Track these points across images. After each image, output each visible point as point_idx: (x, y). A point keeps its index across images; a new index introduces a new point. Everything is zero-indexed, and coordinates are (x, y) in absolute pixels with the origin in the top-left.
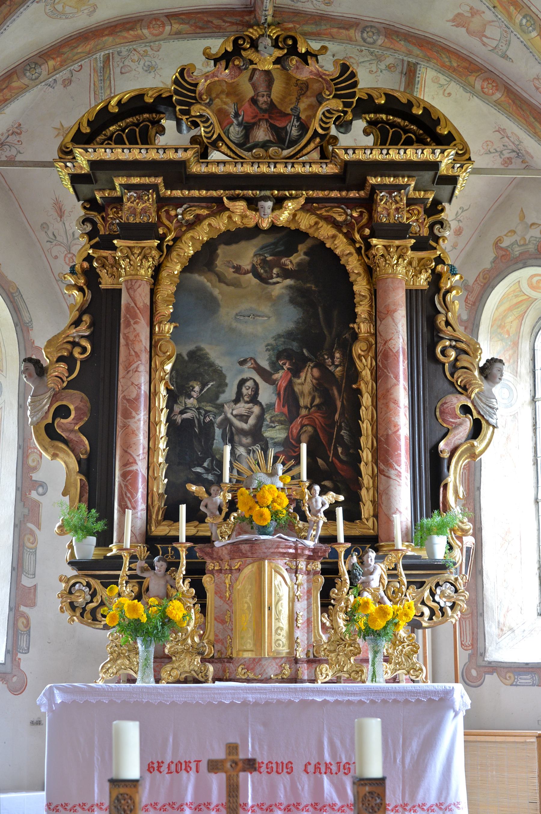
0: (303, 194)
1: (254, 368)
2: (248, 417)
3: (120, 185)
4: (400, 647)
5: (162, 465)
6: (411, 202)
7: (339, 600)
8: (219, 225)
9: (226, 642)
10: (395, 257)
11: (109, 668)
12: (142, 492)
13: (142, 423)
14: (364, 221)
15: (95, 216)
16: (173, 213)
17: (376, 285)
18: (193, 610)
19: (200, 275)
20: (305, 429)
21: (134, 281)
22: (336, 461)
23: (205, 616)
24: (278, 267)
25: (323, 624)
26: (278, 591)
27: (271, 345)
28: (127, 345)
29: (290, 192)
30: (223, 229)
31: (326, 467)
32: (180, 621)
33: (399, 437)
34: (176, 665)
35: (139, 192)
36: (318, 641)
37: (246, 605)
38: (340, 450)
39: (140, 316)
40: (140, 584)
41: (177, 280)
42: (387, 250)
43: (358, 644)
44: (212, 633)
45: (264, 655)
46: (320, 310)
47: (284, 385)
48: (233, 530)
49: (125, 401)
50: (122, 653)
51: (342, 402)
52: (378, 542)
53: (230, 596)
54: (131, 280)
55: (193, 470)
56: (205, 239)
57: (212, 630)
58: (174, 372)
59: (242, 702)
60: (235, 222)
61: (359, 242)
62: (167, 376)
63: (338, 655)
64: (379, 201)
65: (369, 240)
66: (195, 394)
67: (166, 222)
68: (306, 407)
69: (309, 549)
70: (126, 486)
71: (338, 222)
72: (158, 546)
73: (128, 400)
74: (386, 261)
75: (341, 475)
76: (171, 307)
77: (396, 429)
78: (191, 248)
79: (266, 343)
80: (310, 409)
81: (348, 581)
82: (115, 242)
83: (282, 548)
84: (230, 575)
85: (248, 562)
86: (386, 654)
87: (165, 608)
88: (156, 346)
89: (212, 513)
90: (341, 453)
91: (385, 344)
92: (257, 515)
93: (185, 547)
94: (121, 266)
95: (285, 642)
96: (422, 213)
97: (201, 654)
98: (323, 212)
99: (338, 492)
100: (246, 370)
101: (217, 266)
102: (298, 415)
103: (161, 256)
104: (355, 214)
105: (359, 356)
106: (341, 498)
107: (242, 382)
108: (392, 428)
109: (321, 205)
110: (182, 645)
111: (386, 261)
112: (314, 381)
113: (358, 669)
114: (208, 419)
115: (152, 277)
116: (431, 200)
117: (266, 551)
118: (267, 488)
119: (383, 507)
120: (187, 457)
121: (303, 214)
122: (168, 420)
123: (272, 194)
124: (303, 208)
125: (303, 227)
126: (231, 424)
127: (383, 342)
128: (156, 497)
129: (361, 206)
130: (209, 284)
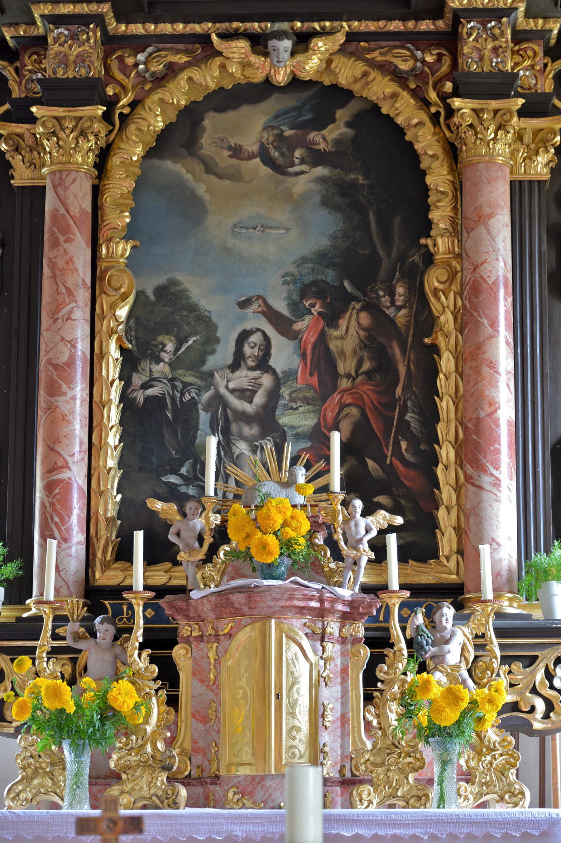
0: (342, 27)
1: (263, 313)
2: (254, 392)
3: (41, 16)
4: (489, 758)
5: (112, 472)
6: (523, 36)
7: (390, 683)
8: (205, 80)
9: (210, 751)
10: (492, 128)
11: (20, 792)
12: (79, 515)
13: (78, 402)
14: (445, 68)
15: (4, 68)
16: (130, 61)
17: (462, 174)
18: (154, 700)
19: (175, 162)
20: (346, 411)
21: (65, 173)
22: (397, 463)
23: (176, 711)
24: (302, 147)
25: (368, 724)
26: (292, 668)
27: (292, 274)
28: (54, 276)
29: (322, 23)
30: (213, 86)
31: (381, 473)
32: (131, 715)
33: (497, 422)
34: (128, 787)
35: (73, 27)
36: (360, 751)
37: (241, 692)
38: (404, 445)
39: (74, 228)
40: (74, 661)
41: (138, 171)
42: (478, 117)
43: (421, 753)
44: (188, 738)
45: (270, 771)
46: (372, 216)
47: (313, 340)
48: (223, 573)
49: (51, 368)
50: (41, 768)
51: (408, 366)
52: (463, 594)
53: (215, 677)
54: (60, 171)
55: (164, 479)
56: (183, 103)
57: (189, 733)
58: (132, 321)
59: (225, 838)
60: (232, 75)
61: (437, 105)
62: (121, 327)
63: (389, 770)
64: (465, 36)
65: (448, 101)
66: (166, 357)
67: (119, 76)
68: (348, 376)
69: (344, 602)
70: (52, 504)
71: (401, 71)
72: (107, 603)
73: (56, 367)
74: (476, 135)
75: (405, 486)
76: (127, 214)
77: (493, 409)
78: (159, 119)
79: (283, 272)
80: (354, 379)
81: (405, 652)
82: (34, 109)
83: (298, 599)
84: (215, 644)
85: (243, 623)
86: (465, 768)
87: (107, 692)
88: (102, 279)
89: (187, 545)
90: (406, 450)
91: (475, 270)
92: (257, 546)
93: (142, 598)
94: (45, 148)
95: (303, 751)
96: (541, 54)
97: (167, 768)
98: (376, 55)
99: (393, 511)
100: (251, 315)
101: (202, 147)
102: (335, 388)
103: (111, 132)
104: (429, 59)
105: (436, 292)
106: (399, 520)
107: (244, 336)
108: (486, 407)
109: (373, 45)
110: (136, 755)
111: (476, 135)
112: (362, 333)
113: (420, 793)
114: (187, 397)
115: (96, 166)
116: (556, 32)
117: (272, 604)
118: (274, 502)
119: (471, 536)
120: (154, 459)
121: (344, 60)
122: (124, 398)
123: (292, 28)
124: (342, 50)
125: (343, 81)
126: (226, 405)
127: (472, 268)
128: (102, 525)
129: (439, 45)
130: (189, 177)
